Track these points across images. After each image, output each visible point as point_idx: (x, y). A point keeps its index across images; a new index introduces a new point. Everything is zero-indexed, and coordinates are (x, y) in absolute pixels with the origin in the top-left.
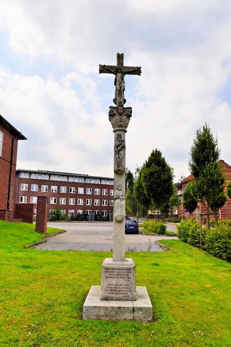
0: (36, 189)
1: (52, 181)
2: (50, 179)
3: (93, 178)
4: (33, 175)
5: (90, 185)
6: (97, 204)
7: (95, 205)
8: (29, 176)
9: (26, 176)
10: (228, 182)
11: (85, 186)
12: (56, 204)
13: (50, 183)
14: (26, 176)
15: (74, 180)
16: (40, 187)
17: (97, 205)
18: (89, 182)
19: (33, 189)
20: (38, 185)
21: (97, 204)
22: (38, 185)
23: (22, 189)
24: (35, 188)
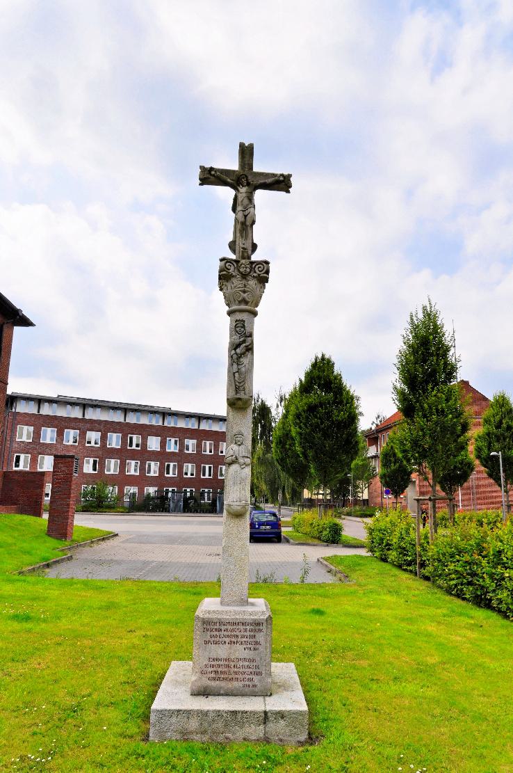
0: (52, 439)
1: (91, 421)
5: (175, 432)
14: (31, 409)
15: (138, 419)
24: (114, 441)
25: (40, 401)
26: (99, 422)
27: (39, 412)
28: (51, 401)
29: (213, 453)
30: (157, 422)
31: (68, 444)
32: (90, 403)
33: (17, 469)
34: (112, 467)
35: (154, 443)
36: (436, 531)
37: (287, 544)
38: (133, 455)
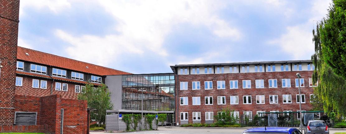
0: (198, 87)
1: (219, 75)
2: (240, 72)
3: (229, 65)
4: (193, 69)
5: (246, 76)
6: (197, 118)
7: (284, 103)
8: (213, 71)
9: (185, 72)
10: (345, 15)
11: (292, 75)
12: (251, 104)
13: (292, 75)
14: (185, 72)
15: (206, 72)
16: (202, 84)
17: (287, 102)
18: (272, 71)
19: (194, 88)
20: (200, 82)
21: (197, 118)
22: (200, 82)
23: (193, 88)
24: (234, 85)
25: (190, 67)
26: (224, 75)
27: (214, 73)
28: (221, 66)
29: (310, 86)
30: (261, 70)
31: (219, 89)
32: (241, 64)
33: (182, 105)
34: (234, 100)
35: (260, 84)
36: (174, 112)
37: (175, 127)
38: (247, 91)
